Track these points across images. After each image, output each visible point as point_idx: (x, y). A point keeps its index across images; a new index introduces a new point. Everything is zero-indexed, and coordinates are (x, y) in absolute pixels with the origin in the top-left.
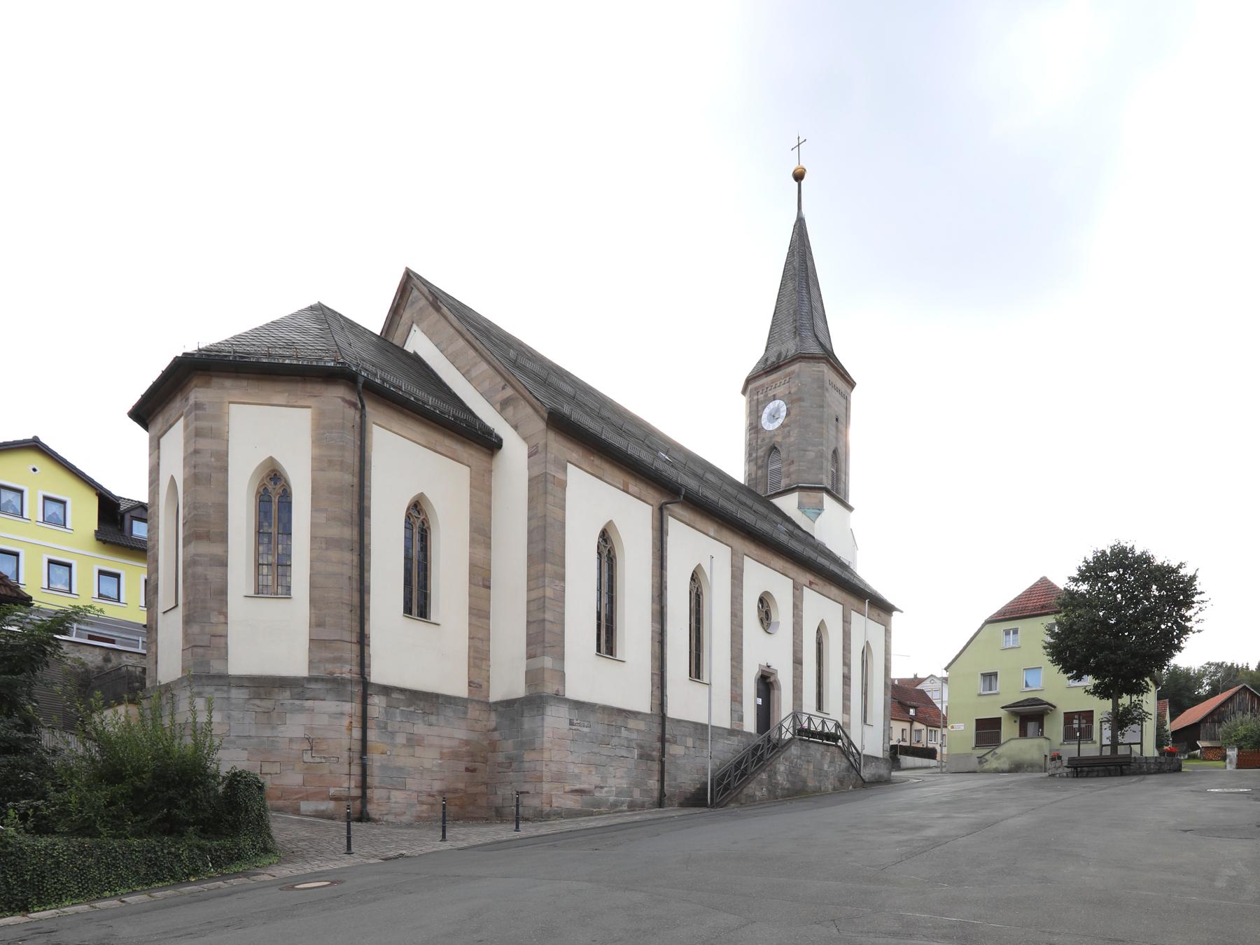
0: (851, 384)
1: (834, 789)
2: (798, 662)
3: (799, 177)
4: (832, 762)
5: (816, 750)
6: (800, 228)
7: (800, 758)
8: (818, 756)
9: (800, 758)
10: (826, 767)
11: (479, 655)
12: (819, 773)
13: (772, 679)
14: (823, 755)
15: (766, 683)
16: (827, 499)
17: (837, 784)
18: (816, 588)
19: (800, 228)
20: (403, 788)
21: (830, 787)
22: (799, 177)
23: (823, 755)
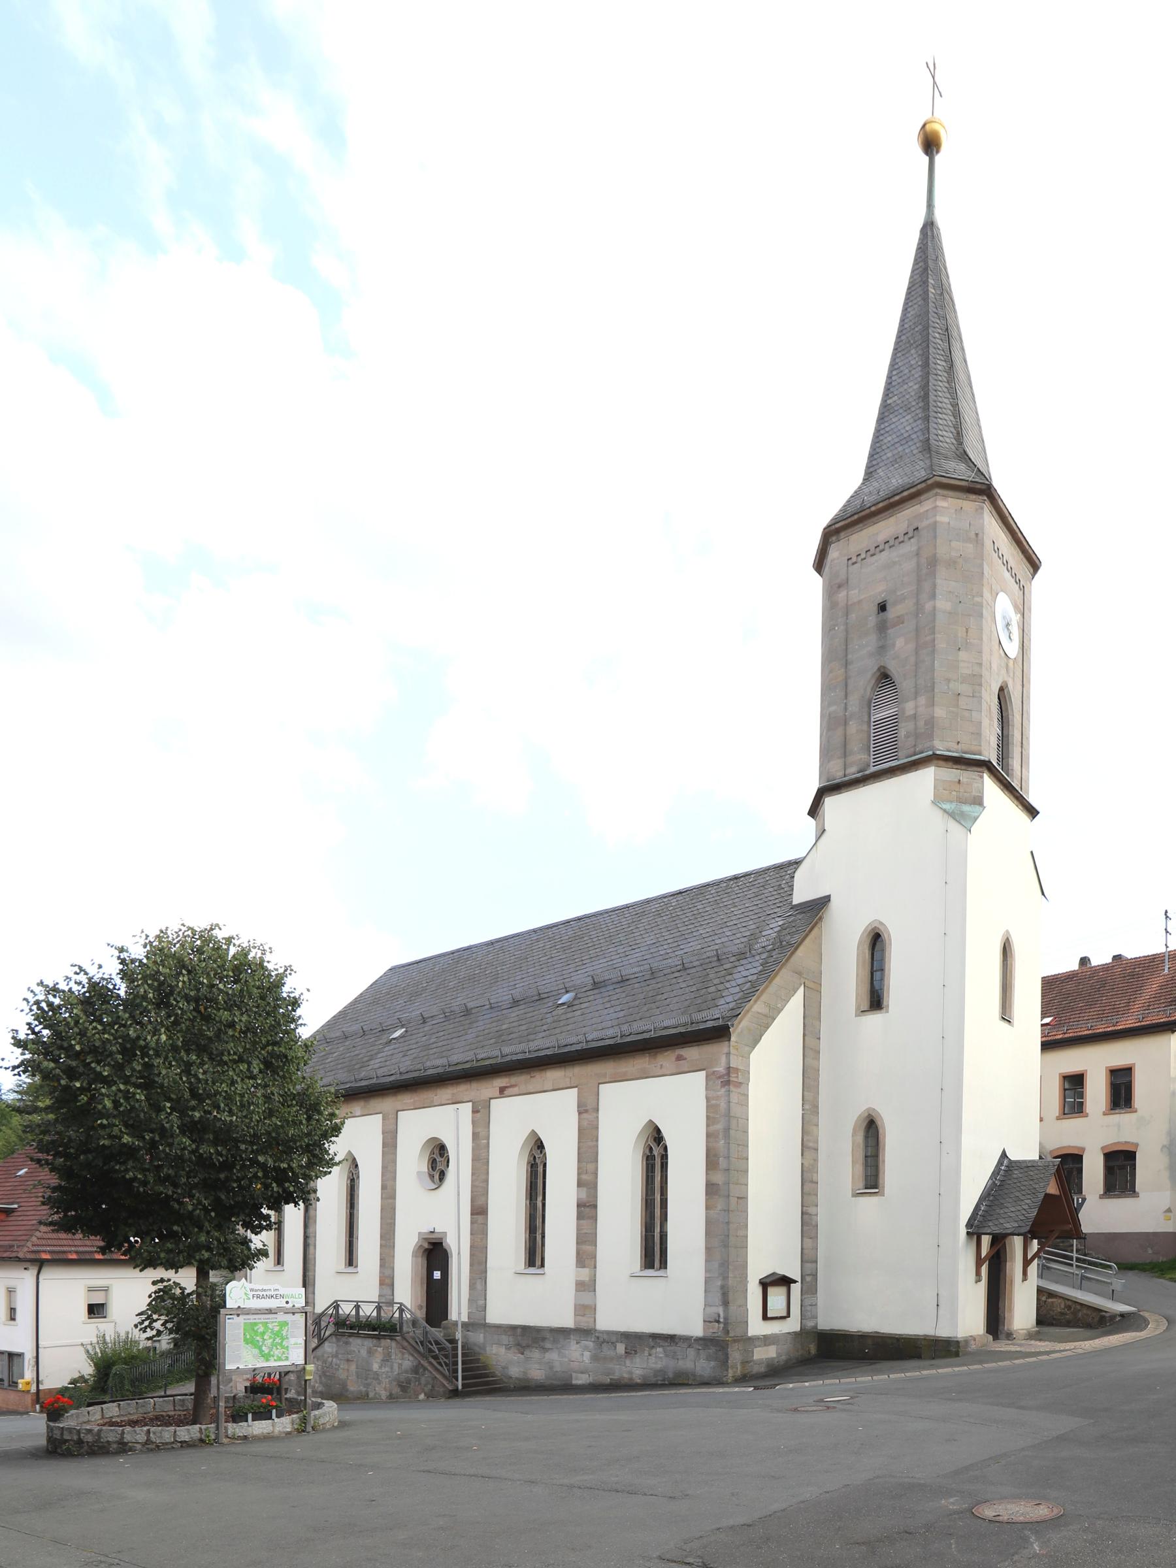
0: (1034, 565)
1: (390, 1396)
2: (479, 1211)
3: (930, 144)
4: (386, 1359)
5: (360, 1346)
6: (929, 230)
7: (336, 1356)
8: (364, 1353)
9: (336, 1356)
10: (375, 1367)
11: (387, 1281)
12: (364, 1373)
13: (426, 1246)
14: (370, 1352)
15: (434, 1253)
16: (990, 788)
17: (396, 1390)
18: (515, 1090)
19: (929, 230)
20: (188, 1055)
21: (384, 1395)
22: (930, 144)
23: (370, 1352)
